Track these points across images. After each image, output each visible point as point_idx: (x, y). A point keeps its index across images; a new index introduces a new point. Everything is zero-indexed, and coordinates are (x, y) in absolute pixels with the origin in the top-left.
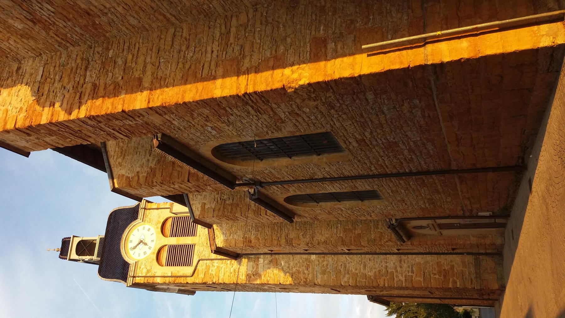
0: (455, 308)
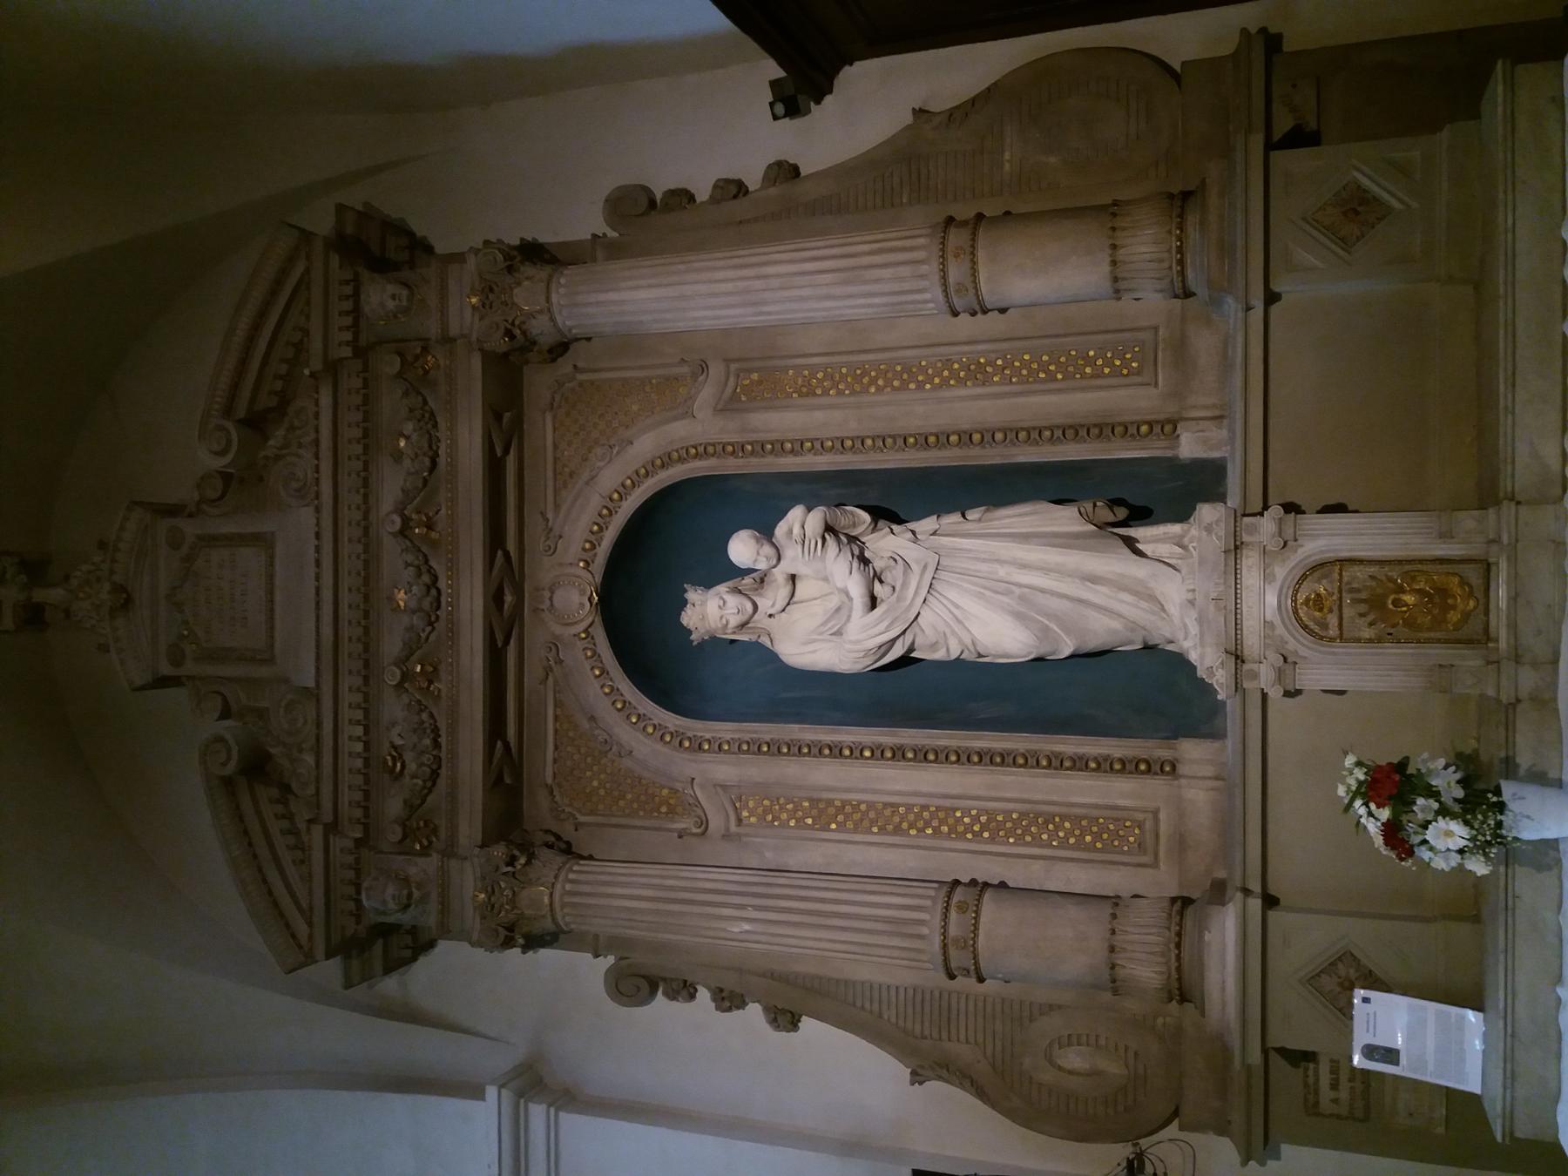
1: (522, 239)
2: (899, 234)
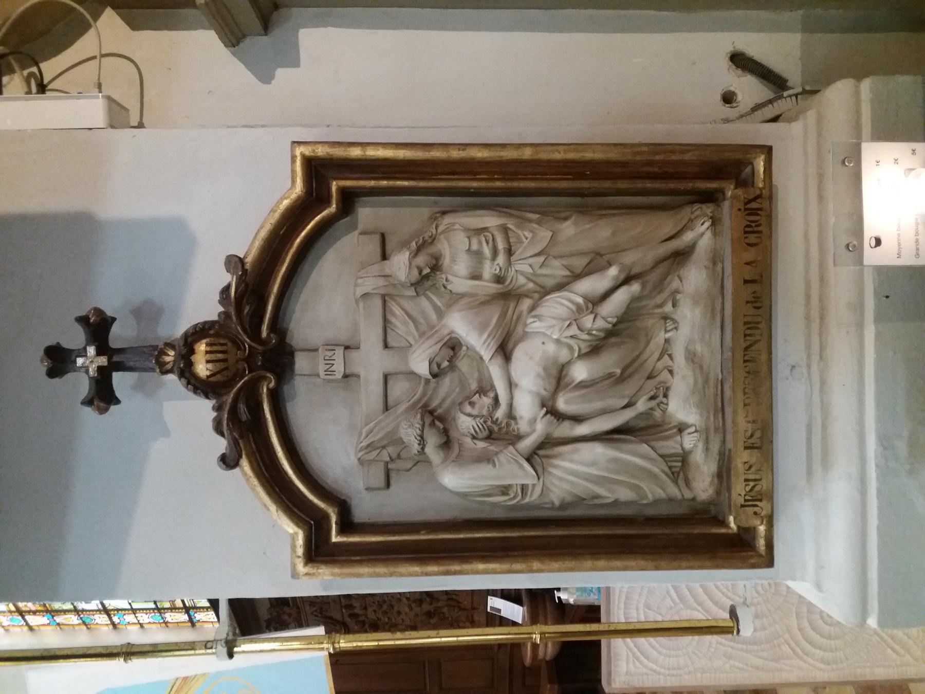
1: (58, 343)
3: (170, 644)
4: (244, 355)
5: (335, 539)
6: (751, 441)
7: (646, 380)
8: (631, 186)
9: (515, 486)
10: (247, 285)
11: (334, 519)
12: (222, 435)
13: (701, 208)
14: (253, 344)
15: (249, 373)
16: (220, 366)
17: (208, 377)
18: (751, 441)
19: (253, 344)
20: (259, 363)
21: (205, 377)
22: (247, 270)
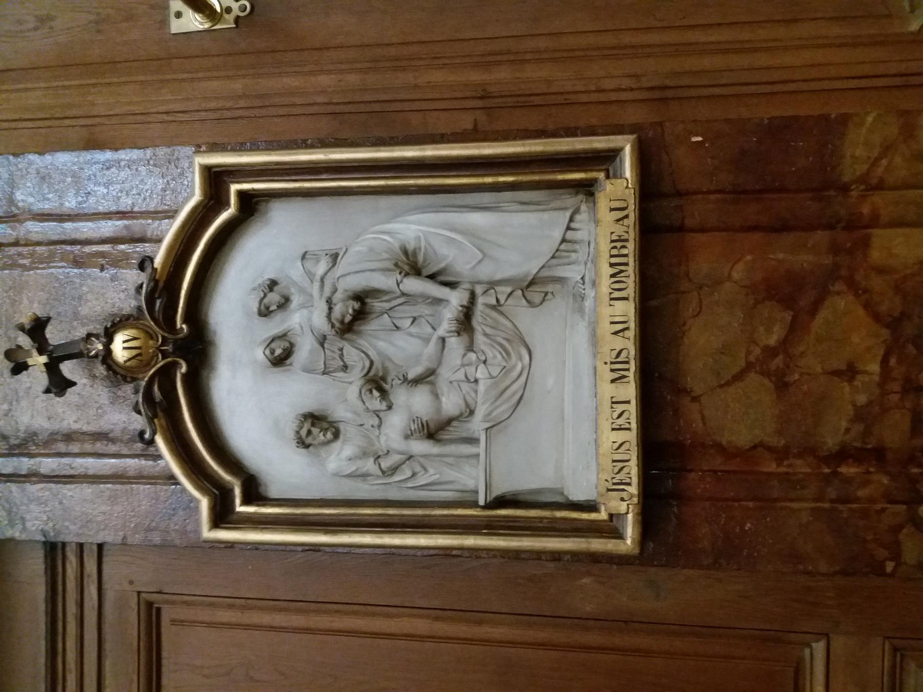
0: (110, 435)
2: (533, 513)
3: (398, 505)
4: (156, 344)
5: (240, 509)
6: (618, 477)
7: (379, 430)
8: (494, 180)
9: (72, 558)
10: (156, 282)
11: (237, 491)
12: (139, 413)
13: (627, 187)
14: (166, 335)
15: (163, 359)
16: (134, 352)
17: (125, 362)
18: (618, 477)
19: (166, 335)
20: (672, 205)
21: (123, 362)
22: (156, 269)
